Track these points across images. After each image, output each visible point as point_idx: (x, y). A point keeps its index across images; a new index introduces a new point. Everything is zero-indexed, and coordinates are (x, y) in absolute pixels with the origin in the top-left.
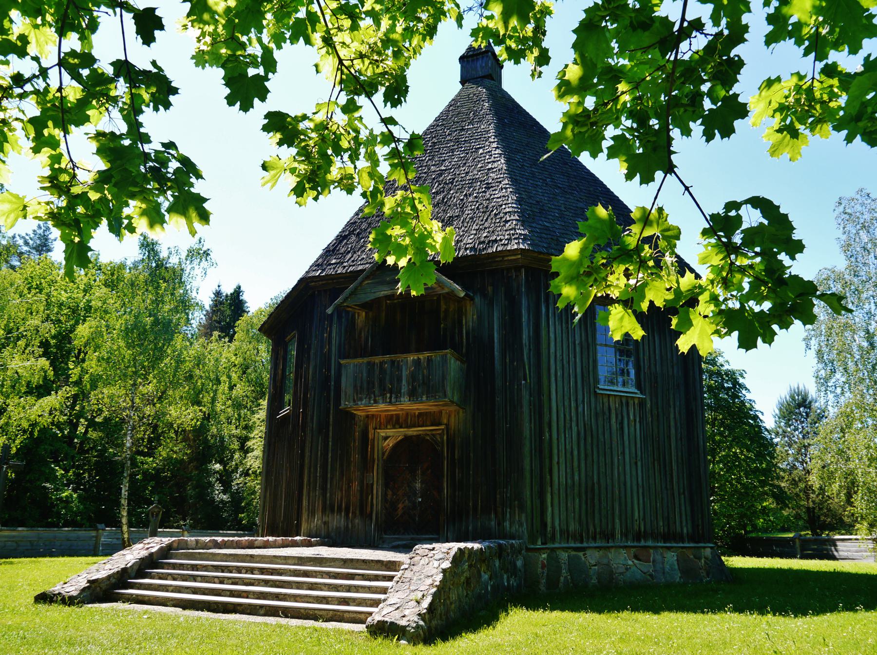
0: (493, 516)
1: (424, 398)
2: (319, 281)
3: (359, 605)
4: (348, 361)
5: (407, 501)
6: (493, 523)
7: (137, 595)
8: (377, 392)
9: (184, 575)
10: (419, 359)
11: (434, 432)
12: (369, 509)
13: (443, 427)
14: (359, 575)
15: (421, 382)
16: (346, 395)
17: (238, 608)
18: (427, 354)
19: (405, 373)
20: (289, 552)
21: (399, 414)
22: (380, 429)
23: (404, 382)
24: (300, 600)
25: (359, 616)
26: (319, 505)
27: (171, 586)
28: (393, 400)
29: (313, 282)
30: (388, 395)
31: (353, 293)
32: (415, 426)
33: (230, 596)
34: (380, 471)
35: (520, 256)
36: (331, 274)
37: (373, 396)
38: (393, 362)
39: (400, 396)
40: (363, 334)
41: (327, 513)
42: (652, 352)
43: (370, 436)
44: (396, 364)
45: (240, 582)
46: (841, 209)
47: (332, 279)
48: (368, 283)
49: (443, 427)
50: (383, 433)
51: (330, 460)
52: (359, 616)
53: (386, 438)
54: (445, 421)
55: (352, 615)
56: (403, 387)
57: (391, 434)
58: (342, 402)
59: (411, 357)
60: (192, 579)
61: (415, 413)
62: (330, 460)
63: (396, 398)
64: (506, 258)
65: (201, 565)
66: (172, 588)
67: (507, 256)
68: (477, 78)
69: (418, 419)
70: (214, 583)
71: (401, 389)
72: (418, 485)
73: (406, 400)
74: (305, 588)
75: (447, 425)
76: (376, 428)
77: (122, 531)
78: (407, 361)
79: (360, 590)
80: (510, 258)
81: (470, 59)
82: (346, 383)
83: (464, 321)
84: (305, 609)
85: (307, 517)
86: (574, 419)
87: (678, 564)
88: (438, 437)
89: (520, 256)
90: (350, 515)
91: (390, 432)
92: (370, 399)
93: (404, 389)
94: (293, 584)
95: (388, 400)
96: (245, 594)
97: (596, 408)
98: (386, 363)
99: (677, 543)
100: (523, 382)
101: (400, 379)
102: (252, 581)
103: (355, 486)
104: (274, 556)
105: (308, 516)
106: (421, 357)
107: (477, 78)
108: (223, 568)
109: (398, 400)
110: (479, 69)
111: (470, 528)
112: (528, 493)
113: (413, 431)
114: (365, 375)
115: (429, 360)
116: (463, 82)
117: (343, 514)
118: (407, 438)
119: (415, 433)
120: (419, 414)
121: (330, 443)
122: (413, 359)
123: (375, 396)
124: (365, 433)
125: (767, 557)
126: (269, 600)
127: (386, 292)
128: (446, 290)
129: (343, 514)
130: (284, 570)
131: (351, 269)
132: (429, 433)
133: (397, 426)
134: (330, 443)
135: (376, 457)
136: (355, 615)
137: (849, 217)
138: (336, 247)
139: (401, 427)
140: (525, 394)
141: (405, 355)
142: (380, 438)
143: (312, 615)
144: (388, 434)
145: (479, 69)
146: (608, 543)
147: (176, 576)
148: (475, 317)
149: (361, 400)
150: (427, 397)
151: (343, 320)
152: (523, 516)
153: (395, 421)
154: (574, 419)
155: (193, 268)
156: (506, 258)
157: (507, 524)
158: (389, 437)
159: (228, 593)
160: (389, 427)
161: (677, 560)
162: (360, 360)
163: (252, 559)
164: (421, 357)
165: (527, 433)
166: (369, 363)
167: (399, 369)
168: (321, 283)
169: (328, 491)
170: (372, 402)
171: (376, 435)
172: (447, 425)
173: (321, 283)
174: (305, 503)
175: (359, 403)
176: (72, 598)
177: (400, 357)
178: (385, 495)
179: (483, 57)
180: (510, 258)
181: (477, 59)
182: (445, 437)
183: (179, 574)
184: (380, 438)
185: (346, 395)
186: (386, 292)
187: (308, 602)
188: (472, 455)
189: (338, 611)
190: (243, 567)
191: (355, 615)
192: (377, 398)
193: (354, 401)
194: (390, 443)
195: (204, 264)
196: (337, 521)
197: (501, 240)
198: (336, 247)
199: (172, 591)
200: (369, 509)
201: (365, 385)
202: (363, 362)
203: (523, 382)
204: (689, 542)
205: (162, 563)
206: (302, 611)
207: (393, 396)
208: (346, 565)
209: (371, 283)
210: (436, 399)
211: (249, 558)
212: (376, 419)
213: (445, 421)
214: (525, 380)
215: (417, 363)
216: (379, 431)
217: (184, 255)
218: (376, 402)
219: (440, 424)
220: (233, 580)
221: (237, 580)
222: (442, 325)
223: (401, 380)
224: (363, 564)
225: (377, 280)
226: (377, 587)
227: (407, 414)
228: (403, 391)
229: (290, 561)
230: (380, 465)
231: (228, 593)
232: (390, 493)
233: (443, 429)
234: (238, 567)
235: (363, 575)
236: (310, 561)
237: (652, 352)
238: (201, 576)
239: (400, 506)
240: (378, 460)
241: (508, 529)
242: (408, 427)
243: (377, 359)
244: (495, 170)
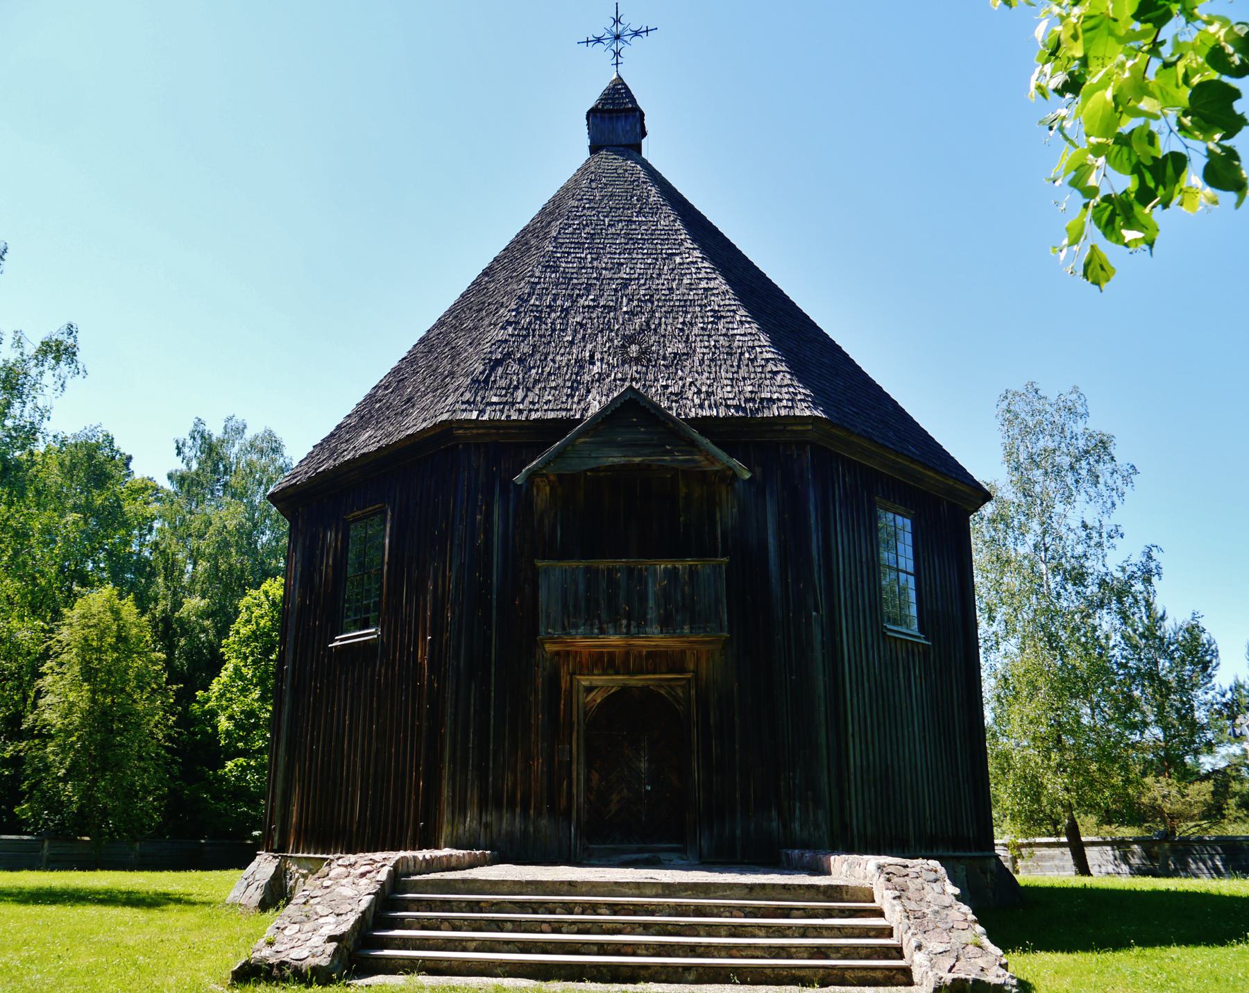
0: (774, 813)
1: (686, 629)
2: (473, 428)
3: (845, 957)
4: (551, 563)
5: (625, 791)
6: (774, 824)
7: (424, 959)
8: (604, 616)
9: (475, 920)
10: (675, 568)
11: (672, 683)
12: (564, 802)
13: (689, 676)
14: (798, 909)
15: (680, 604)
16: (548, 616)
17: (642, 972)
18: (690, 562)
19: (651, 590)
20: (629, 876)
21: (613, 652)
22: (580, 674)
23: (651, 603)
24: (738, 954)
25: (872, 974)
26: (473, 796)
27: (473, 940)
28: (633, 630)
29: (460, 429)
30: (624, 622)
31: (560, 454)
32: (642, 673)
33: (598, 954)
34: (582, 742)
35: (810, 427)
36: (499, 420)
37: (597, 622)
38: (630, 571)
39: (645, 625)
40: (546, 522)
41: (490, 808)
42: (933, 581)
43: (563, 685)
44: (636, 573)
45: (595, 928)
46: (1004, 405)
47: (498, 428)
48: (585, 442)
49: (689, 676)
50: (585, 681)
51: (492, 722)
52: (872, 974)
53: (589, 689)
54: (691, 667)
55: (860, 974)
56: (650, 611)
57: (600, 684)
58: (542, 629)
59: (662, 566)
60: (494, 927)
61: (640, 652)
62: (492, 722)
63: (638, 626)
64: (790, 428)
65: (486, 901)
66: (474, 944)
67: (791, 425)
68: (617, 146)
69: (647, 662)
70: (542, 932)
71: (646, 614)
72: (643, 765)
73: (656, 631)
74: (723, 933)
75: (696, 672)
76: (574, 673)
77: (43, 846)
78: (655, 570)
79: (825, 933)
80: (795, 428)
81: (606, 116)
82: (548, 598)
83: (718, 516)
84: (773, 968)
85: (450, 816)
86: (865, 671)
87: (967, 881)
88: (680, 692)
89: (810, 427)
90: (532, 812)
91: (598, 680)
92: (592, 625)
93: (651, 615)
94: (699, 928)
95: (624, 630)
96: (630, 950)
97: (885, 656)
98: (618, 571)
99: (965, 851)
100: (814, 614)
101: (643, 598)
102: (619, 926)
103: (538, 765)
104: (616, 883)
105: (453, 813)
106: (679, 565)
107: (617, 146)
108: (535, 906)
109: (641, 630)
110: (621, 133)
111: (738, 832)
112: (826, 780)
113: (637, 680)
114: (581, 587)
115: (692, 572)
116: (594, 149)
117: (518, 810)
118: (625, 690)
119: (640, 684)
120: (648, 653)
121: (493, 694)
122: (665, 568)
123: (601, 623)
124: (554, 680)
125: (102, 869)
126: (678, 956)
127: (616, 460)
128: (717, 467)
129: (518, 810)
130: (658, 905)
131: (534, 416)
132: (664, 684)
133: (611, 671)
134: (493, 694)
135: (575, 718)
136: (864, 973)
137: (1011, 417)
138: (489, 376)
139: (617, 673)
140: (817, 631)
141: (652, 561)
142: (581, 689)
143: (787, 976)
144: (595, 683)
145: (621, 133)
146: (932, 852)
147: (457, 923)
148: (735, 510)
149: (576, 626)
150: (691, 629)
151: (512, 495)
152: (820, 814)
153: (605, 662)
154: (865, 671)
155: (41, 373)
156: (790, 428)
157: (797, 825)
158: (596, 687)
159: (595, 948)
160: (596, 672)
161: (967, 876)
162: (574, 564)
163: (573, 889)
164: (679, 565)
165: (821, 690)
166: (588, 569)
167: (642, 581)
168: (475, 431)
169: (491, 772)
170: (596, 631)
171: (575, 683)
172: (696, 672)
173: (475, 431)
174: (446, 792)
175: (573, 632)
176: (316, 969)
177: (642, 563)
178: (588, 780)
179: (626, 117)
180: (795, 428)
181: (618, 118)
182: (693, 692)
183: (465, 919)
184: (581, 689)
185: (548, 616)
186: (616, 460)
187: (753, 957)
188: (737, 720)
189: (833, 967)
190: (576, 903)
191: (864, 973)
192: (605, 626)
193: (564, 628)
194: (598, 697)
195: (64, 367)
196: (508, 823)
197: (780, 400)
198: (489, 376)
199: (476, 950)
200: (564, 802)
201: (583, 604)
202: (577, 567)
203: (814, 614)
204: (975, 851)
205: (404, 899)
206: (768, 971)
207: (633, 623)
208: (754, 894)
209: (589, 443)
210: (705, 631)
211: (565, 888)
212: (575, 658)
213: (691, 667)
214: (817, 610)
215: (672, 574)
216: (578, 677)
217: (30, 349)
218: (602, 631)
219: (682, 670)
220: (581, 926)
221: (589, 926)
222: (682, 519)
223: (646, 600)
224: (784, 891)
225: (599, 439)
226: (853, 927)
227: (627, 653)
228: (649, 617)
229: (647, 892)
230: (582, 733)
231: (595, 948)
232: (595, 777)
233: (689, 679)
234: (564, 903)
235: (804, 909)
236: (686, 890)
237: (933, 581)
238: (512, 921)
239: (615, 797)
240: (578, 724)
241: (798, 833)
242: (628, 672)
243: (603, 564)
244: (715, 291)
